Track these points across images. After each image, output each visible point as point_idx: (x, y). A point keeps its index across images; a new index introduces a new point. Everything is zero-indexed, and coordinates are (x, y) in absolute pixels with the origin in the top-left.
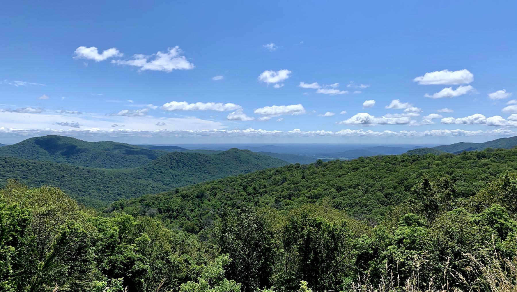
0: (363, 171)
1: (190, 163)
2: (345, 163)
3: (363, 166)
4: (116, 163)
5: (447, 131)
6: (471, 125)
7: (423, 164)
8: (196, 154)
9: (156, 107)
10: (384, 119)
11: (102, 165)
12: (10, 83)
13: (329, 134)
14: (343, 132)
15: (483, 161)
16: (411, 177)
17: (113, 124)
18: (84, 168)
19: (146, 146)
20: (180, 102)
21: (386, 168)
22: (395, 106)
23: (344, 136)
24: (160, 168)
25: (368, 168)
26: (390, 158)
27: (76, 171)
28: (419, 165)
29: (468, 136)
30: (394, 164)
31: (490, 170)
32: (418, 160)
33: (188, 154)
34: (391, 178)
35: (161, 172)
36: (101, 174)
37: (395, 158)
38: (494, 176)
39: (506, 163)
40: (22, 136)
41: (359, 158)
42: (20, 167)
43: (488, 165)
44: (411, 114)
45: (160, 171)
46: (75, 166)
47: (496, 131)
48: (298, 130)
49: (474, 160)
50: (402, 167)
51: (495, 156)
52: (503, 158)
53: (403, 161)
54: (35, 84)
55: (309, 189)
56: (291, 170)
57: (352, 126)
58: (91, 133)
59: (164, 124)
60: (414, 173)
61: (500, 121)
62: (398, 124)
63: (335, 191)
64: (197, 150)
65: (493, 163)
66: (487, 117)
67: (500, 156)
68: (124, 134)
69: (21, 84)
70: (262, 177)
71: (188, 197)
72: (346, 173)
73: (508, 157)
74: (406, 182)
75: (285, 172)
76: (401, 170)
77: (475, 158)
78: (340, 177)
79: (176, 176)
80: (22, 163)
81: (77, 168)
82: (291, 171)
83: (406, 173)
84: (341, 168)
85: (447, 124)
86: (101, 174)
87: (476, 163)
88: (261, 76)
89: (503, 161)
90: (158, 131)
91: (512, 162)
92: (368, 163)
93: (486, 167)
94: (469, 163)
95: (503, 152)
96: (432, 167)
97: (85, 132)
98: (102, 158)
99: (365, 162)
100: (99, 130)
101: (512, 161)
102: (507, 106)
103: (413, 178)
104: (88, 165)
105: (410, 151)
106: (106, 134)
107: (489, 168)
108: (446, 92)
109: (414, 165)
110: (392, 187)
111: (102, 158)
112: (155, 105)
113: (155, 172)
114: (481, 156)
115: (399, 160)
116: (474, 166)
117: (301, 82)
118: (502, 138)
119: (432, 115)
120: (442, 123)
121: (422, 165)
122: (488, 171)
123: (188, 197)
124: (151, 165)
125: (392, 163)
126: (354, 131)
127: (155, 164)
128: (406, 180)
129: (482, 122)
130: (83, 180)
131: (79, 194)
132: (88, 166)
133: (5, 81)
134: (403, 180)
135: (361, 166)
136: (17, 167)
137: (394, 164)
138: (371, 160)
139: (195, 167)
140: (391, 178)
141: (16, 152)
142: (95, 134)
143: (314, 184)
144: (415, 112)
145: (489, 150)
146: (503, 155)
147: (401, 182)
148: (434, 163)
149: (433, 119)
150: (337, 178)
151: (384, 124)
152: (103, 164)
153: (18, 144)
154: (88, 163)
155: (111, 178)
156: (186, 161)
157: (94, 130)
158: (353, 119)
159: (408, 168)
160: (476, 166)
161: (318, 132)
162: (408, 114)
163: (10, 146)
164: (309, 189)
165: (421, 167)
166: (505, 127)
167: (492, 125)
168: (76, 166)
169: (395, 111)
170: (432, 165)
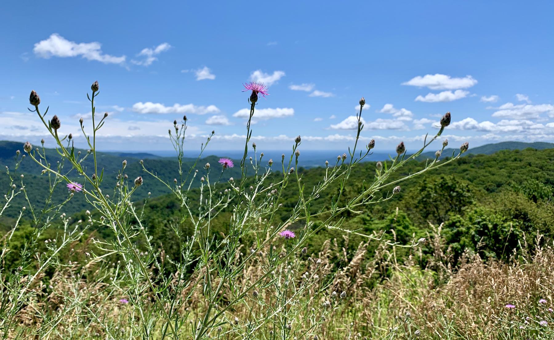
6: (250, 93)
9: (122, 109)
14: (331, 138)
15: (464, 167)
19: (164, 156)
21: (366, 175)
22: (389, 111)
23: (335, 142)
26: (372, 164)
27: (33, 181)
44: (402, 118)
49: (455, 165)
51: (475, 162)
55: (286, 198)
59: (136, 128)
61: (492, 127)
64: (171, 158)
66: (480, 122)
67: (480, 162)
71: (157, 207)
79: (148, 185)
89: (483, 167)
93: (465, 173)
94: (449, 169)
95: (483, 158)
101: (491, 167)
102: (499, 110)
107: (467, 174)
112: (121, 106)
117: (206, 68)
119: (424, 120)
120: (433, 128)
123: (157, 207)
129: (474, 127)
130: (42, 190)
131: (37, 205)
143: (292, 192)
144: (408, 116)
149: (424, 124)
151: (374, 129)
162: (399, 119)
164: (286, 198)
165: (401, 174)
166: (495, 133)
167: (485, 131)
168: (33, 175)
169: (387, 116)
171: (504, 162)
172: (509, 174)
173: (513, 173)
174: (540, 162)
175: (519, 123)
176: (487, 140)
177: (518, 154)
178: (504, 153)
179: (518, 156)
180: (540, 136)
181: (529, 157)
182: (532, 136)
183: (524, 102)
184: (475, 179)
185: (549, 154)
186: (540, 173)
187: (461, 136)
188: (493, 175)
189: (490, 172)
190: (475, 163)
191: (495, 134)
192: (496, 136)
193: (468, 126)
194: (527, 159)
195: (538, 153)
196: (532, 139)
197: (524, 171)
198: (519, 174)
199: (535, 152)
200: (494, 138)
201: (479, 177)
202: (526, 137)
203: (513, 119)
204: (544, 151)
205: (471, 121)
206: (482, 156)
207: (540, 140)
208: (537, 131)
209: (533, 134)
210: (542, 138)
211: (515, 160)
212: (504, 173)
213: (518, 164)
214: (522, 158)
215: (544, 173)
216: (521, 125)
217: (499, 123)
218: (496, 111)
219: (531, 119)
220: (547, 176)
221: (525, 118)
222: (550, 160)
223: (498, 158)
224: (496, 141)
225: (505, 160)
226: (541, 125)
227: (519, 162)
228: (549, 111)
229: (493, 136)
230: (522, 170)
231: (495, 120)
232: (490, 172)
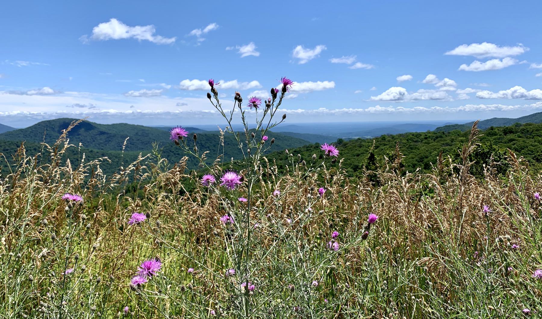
0: (382, 149)
1: (208, 145)
2: (365, 142)
3: (383, 144)
4: (132, 146)
5: (483, 106)
7: (445, 140)
8: (214, 135)
10: (416, 95)
11: (117, 148)
12: (12, 64)
13: (357, 112)
14: (372, 109)
15: (510, 136)
16: (432, 154)
17: (131, 105)
18: (98, 150)
20: (303, 82)
23: (376, 114)
24: (177, 150)
25: (388, 146)
26: (413, 135)
28: (442, 142)
29: (504, 111)
30: (416, 142)
31: (515, 146)
32: (441, 137)
33: (206, 135)
34: (410, 156)
35: (178, 154)
36: (116, 157)
37: (418, 135)
38: (519, 152)
39: (533, 138)
40: (36, 119)
41: (382, 136)
42: (33, 151)
43: (514, 140)
44: (445, 88)
45: (177, 153)
46: (88, 150)
47: (535, 105)
48: (323, 109)
49: (500, 135)
50: (423, 145)
51: (523, 131)
52: (531, 133)
53: (426, 138)
54: (38, 63)
56: (310, 150)
57: (382, 102)
58: (109, 115)
60: (435, 150)
62: (432, 99)
63: (351, 170)
65: (520, 139)
67: (528, 131)
68: (142, 115)
69: (25, 64)
70: (280, 158)
72: (365, 152)
73: (536, 132)
74: (426, 160)
75: (304, 153)
76: (423, 148)
77: (501, 133)
78: (358, 155)
80: (34, 148)
81: (91, 151)
82: (310, 151)
83: (427, 151)
84: (361, 147)
85: (482, 98)
86: (116, 157)
87: (502, 139)
88: (244, 47)
90: (178, 112)
91: (540, 137)
92: (389, 141)
93: (512, 143)
96: (455, 144)
97: (102, 114)
98: (117, 140)
99: (387, 140)
100: (117, 111)
103: (433, 156)
104: (102, 148)
105: (439, 128)
106: (122, 115)
107: (514, 144)
108: (476, 66)
109: (437, 142)
110: (411, 165)
111: (117, 140)
112: (168, 84)
113: (172, 154)
114: (507, 131)
115: (422, 137)
116: (499, 142)
118: (539, 113)
121: (445, 142)
122: (513, 146)
124: (168, 147)
125: (415, 140)
126: (384, 108)
127: (172, 146)
128: (427, 157)
129: (522, 96)
132: (102, 149)
133: (7, 61)
134: (423, 158)
135: (381, 144)
136: (29, 151)
137: (416, 142)
138: (393, 138)
139: (214, 148)
140: (410, 156)
141: (28, 136)
142: (113, 116)
144: (450, 85)
145: (518, 125)
146: (531, 130)
147: (421, 160)
148: (457, 140)
150: (355, 157)
151: (416, 99)
152: (118, 146)
153: (30, 127)
154: (103, 146)
155: (127, 161)
156: (203, 142)
157: (112, 111)
158: (384, 96)
159: (430, 146)
160: (501, 142)
161: (345, 110)
163: (21, 130)
165: (443, 144)
168: (90, 150)
169: (430, 86)
170: (455, 142)
184: (523, 149)
190: (522, 133)
193: (517, 94)
205: (520, 90)
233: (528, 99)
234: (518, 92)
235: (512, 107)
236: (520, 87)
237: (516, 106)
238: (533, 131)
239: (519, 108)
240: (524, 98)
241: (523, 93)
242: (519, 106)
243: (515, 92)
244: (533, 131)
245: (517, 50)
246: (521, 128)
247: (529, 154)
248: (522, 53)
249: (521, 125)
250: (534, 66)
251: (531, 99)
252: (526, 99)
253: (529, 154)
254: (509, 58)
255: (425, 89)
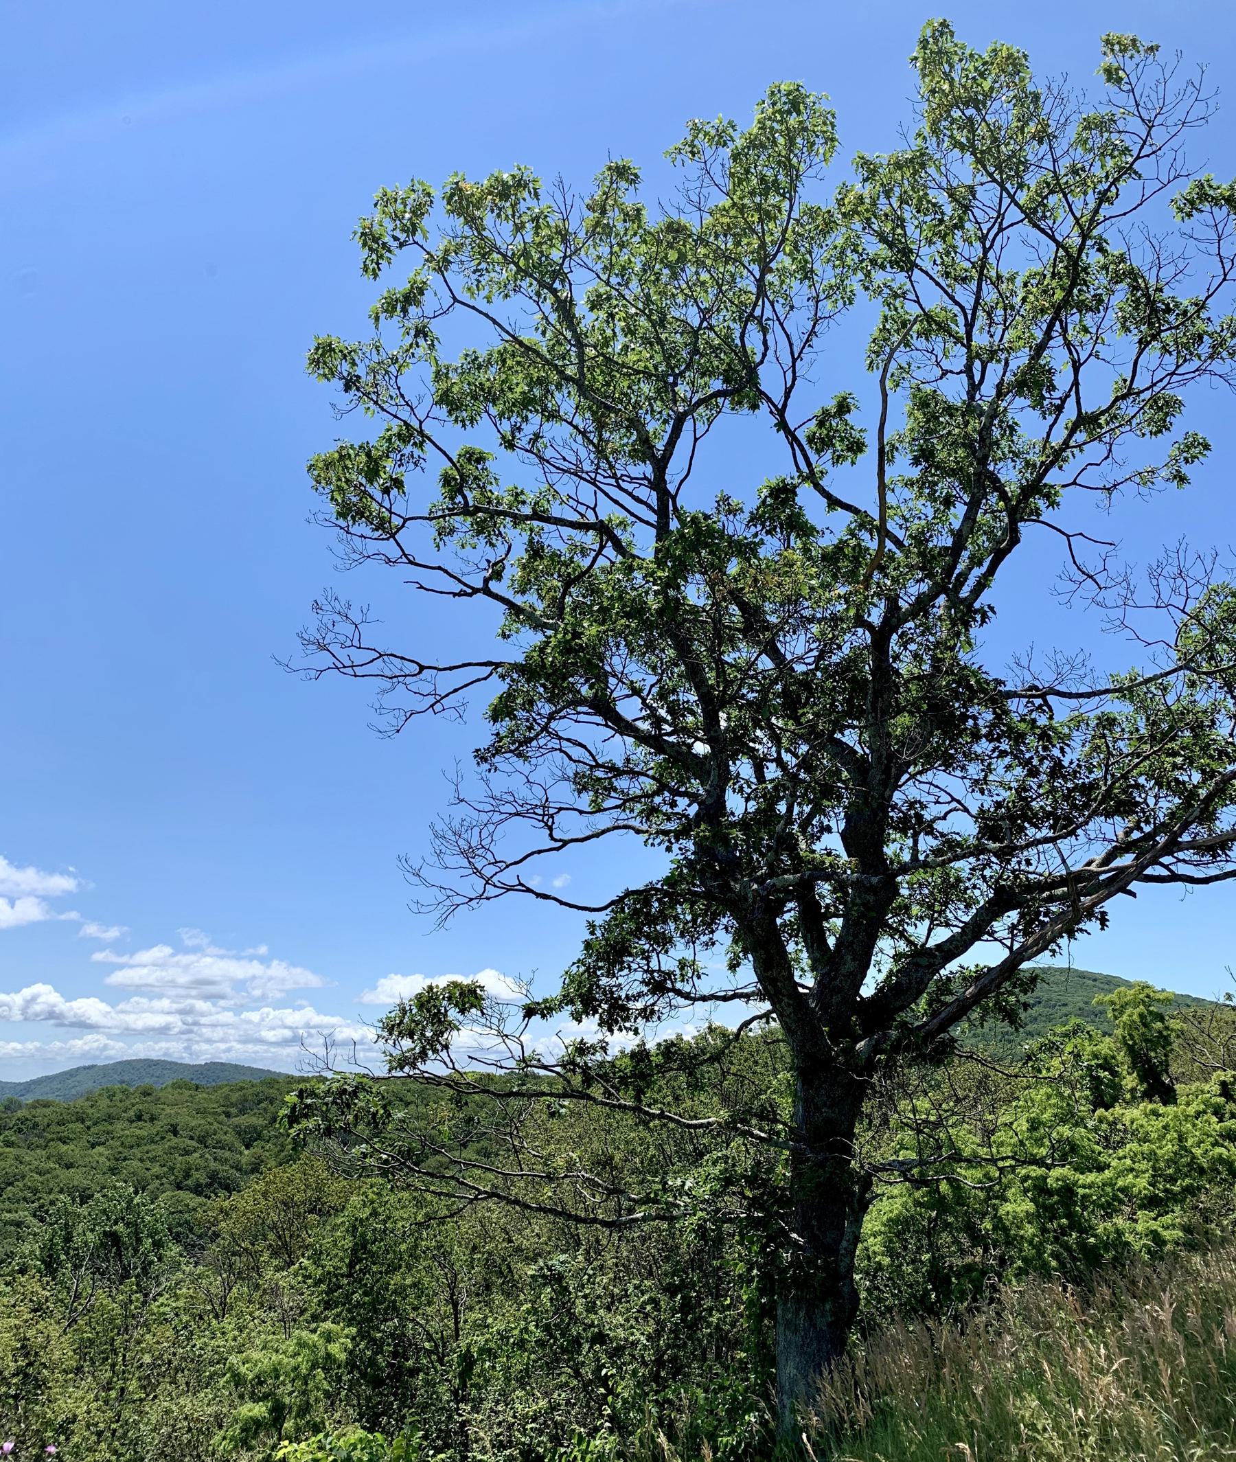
47: (79, 1043)
65: (8, 1150)
66: (69, 999)
67: (36, 1125)
89: (42, 1141)
91: (64, 1143)
95: (47, 1111)
129: (52, 1015)
146: (46, 1121)
167: (83, 1026)
171: (106, 1126)
172: (112, 1163)
173: (125, 1159)
174: (203, 1122)
175: (175, 1006)
176: (84, 1055)
177: (148, 1098)
178: (111, 1096)
179: (146, 1106)
180: (223, 1046)
181: (176, 1109)
182: (204, 1046)
183: (195, 950)
184: (11, 1184)
185: (227, 1097)
186: (196, 1155)
187: (8, 1042)
188: (69, 1166)
189: (59, 1159)
190: (20, 1131)
191: (110, 1036)
192: (111, 1043)
193: (37, 1008)
194: (168, 1114)
195: (201, 1096)
196: (205, 1052)
197: (158, 1150)
198: (141, 1160)
199: (193, 1093)
200: (105, 1047)
201: (23, 1177)
202: (187, 1049)
203: (160, 996)
204: (216, 1090)
205: (46, 995)
206: (46, 1105)
207: (223, 1059)
208: (218, 1033)
209: (209, 1041)
210: (229, 1050)
211: (139, 1118)
212: (102, 1159)
213: (144, 1130)
214: (155, 1110)
215: (207, 1156)
216: (182, 1012)
217: (122, 1006)
218: (121, 967)
219: (207, 997)
220: (213, 1165)
221: (194, 992)
222: (228, 1115)
223: (90, 1111)
224: (107, 1058)
225: (110, 1118)
226: (231, 1014)
227: (148, 1124)
228: (254, 977)
229: (103, 1040)
230: (153, 1146)
231: (116, 996)
232: (59, 1159)
233: (63, 1025)
234: (39, 1000)
235: (19, 1046)
236: (49, 987)
237: (31, 1046)
238: (48, 1125)
239: (37, 1049)
240: (52, 1022)
241: (55, 1006)
242: (37, 1044)
243: (34, 999)
244: (48, 1125)
245: (61, 883)
246: (19, 1114)
247: (24, 1199)
248: (69, 893)
249: (20, 1107)
250: (92, 929)
251: (73, 1025)
252: (57, 1025)
253: (24, 1199)
254: (32, 900)
255: (344, 1018)
